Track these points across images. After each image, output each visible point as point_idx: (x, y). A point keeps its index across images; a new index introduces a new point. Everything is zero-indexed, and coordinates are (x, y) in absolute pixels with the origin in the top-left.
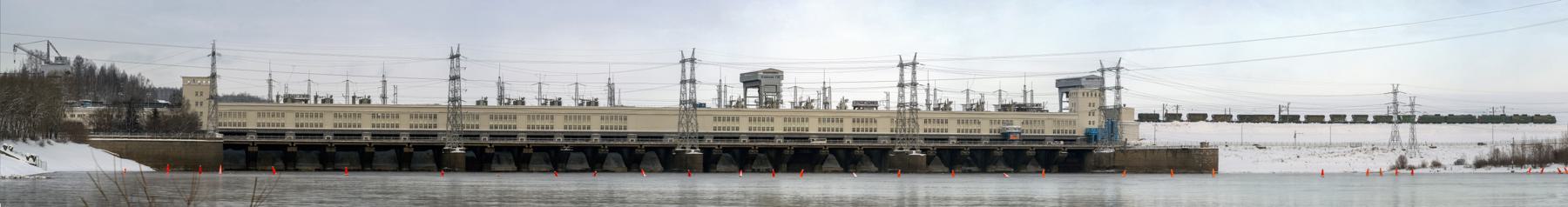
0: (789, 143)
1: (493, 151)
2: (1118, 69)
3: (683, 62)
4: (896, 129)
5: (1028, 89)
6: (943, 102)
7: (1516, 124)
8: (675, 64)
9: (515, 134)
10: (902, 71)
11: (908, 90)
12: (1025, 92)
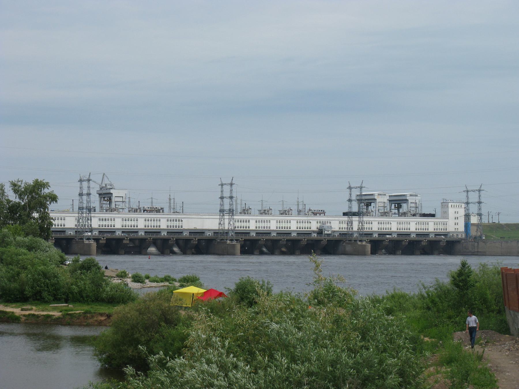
0: (148, 236)
1: (128, 242)
2: (231, 184)
3: (81, 181)
4: (426, 228)
5: (172, 197)
6: (267, 209)
7: (502, 222)
8: (472, 203)
9: (249, 232)
10: (81, 184)
11: (85, 197)
12: (170, 199)
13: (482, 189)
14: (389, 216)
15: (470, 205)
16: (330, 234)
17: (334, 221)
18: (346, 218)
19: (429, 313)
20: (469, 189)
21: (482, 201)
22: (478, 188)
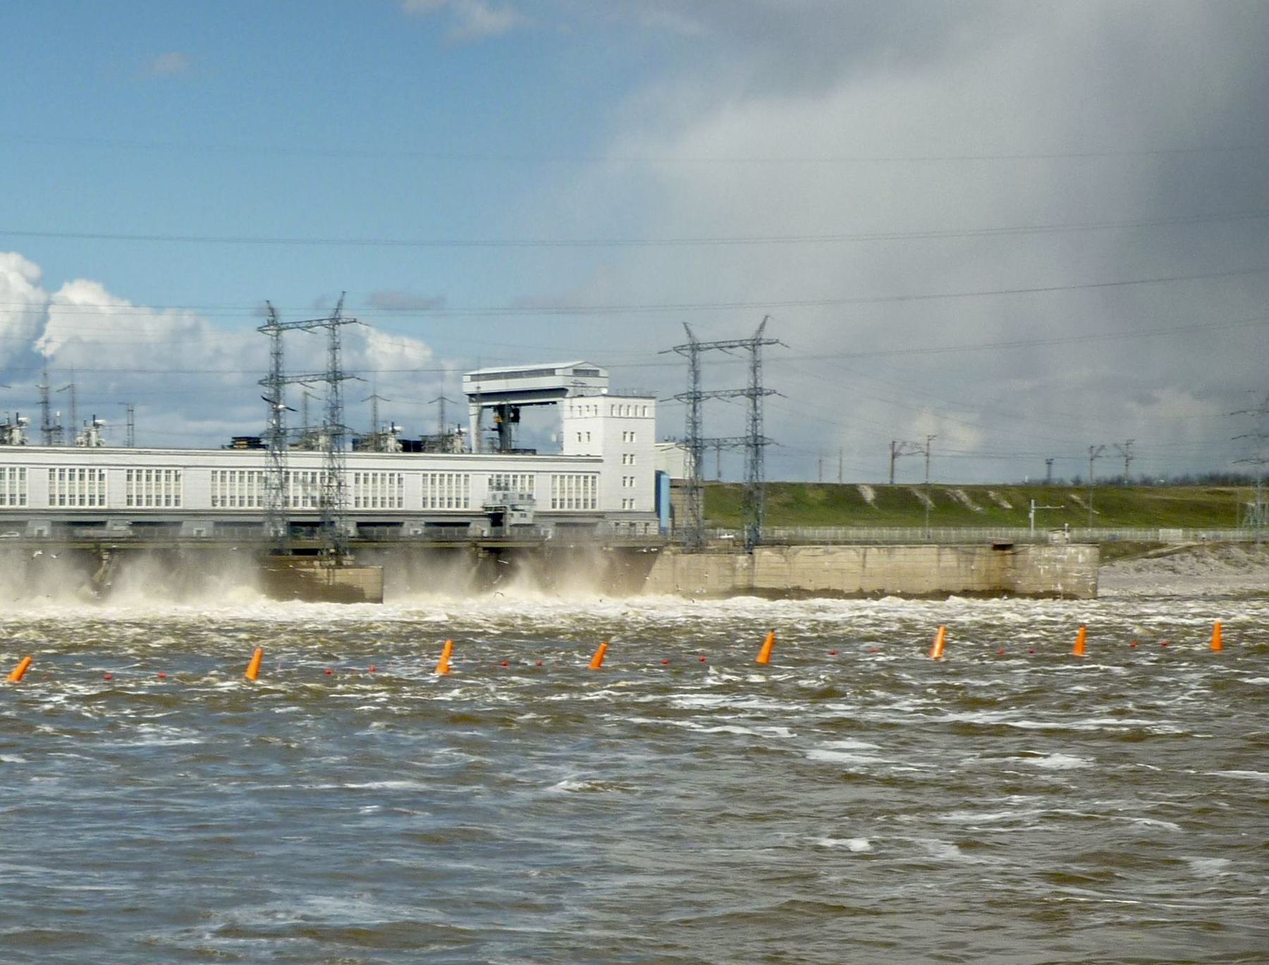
8: (715, 394)
13: (766, 336)
14: (88, 445)
15: (706, 406)
16: (529, 525)
17: (192, 472)
18: (256, 459)
19: (19, 772)
20: (702, 336)
21: (766, 383)
22: (749, 333)
